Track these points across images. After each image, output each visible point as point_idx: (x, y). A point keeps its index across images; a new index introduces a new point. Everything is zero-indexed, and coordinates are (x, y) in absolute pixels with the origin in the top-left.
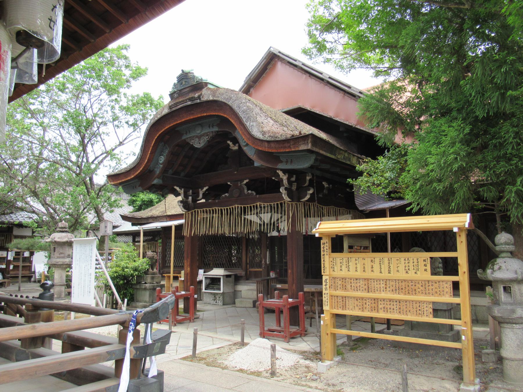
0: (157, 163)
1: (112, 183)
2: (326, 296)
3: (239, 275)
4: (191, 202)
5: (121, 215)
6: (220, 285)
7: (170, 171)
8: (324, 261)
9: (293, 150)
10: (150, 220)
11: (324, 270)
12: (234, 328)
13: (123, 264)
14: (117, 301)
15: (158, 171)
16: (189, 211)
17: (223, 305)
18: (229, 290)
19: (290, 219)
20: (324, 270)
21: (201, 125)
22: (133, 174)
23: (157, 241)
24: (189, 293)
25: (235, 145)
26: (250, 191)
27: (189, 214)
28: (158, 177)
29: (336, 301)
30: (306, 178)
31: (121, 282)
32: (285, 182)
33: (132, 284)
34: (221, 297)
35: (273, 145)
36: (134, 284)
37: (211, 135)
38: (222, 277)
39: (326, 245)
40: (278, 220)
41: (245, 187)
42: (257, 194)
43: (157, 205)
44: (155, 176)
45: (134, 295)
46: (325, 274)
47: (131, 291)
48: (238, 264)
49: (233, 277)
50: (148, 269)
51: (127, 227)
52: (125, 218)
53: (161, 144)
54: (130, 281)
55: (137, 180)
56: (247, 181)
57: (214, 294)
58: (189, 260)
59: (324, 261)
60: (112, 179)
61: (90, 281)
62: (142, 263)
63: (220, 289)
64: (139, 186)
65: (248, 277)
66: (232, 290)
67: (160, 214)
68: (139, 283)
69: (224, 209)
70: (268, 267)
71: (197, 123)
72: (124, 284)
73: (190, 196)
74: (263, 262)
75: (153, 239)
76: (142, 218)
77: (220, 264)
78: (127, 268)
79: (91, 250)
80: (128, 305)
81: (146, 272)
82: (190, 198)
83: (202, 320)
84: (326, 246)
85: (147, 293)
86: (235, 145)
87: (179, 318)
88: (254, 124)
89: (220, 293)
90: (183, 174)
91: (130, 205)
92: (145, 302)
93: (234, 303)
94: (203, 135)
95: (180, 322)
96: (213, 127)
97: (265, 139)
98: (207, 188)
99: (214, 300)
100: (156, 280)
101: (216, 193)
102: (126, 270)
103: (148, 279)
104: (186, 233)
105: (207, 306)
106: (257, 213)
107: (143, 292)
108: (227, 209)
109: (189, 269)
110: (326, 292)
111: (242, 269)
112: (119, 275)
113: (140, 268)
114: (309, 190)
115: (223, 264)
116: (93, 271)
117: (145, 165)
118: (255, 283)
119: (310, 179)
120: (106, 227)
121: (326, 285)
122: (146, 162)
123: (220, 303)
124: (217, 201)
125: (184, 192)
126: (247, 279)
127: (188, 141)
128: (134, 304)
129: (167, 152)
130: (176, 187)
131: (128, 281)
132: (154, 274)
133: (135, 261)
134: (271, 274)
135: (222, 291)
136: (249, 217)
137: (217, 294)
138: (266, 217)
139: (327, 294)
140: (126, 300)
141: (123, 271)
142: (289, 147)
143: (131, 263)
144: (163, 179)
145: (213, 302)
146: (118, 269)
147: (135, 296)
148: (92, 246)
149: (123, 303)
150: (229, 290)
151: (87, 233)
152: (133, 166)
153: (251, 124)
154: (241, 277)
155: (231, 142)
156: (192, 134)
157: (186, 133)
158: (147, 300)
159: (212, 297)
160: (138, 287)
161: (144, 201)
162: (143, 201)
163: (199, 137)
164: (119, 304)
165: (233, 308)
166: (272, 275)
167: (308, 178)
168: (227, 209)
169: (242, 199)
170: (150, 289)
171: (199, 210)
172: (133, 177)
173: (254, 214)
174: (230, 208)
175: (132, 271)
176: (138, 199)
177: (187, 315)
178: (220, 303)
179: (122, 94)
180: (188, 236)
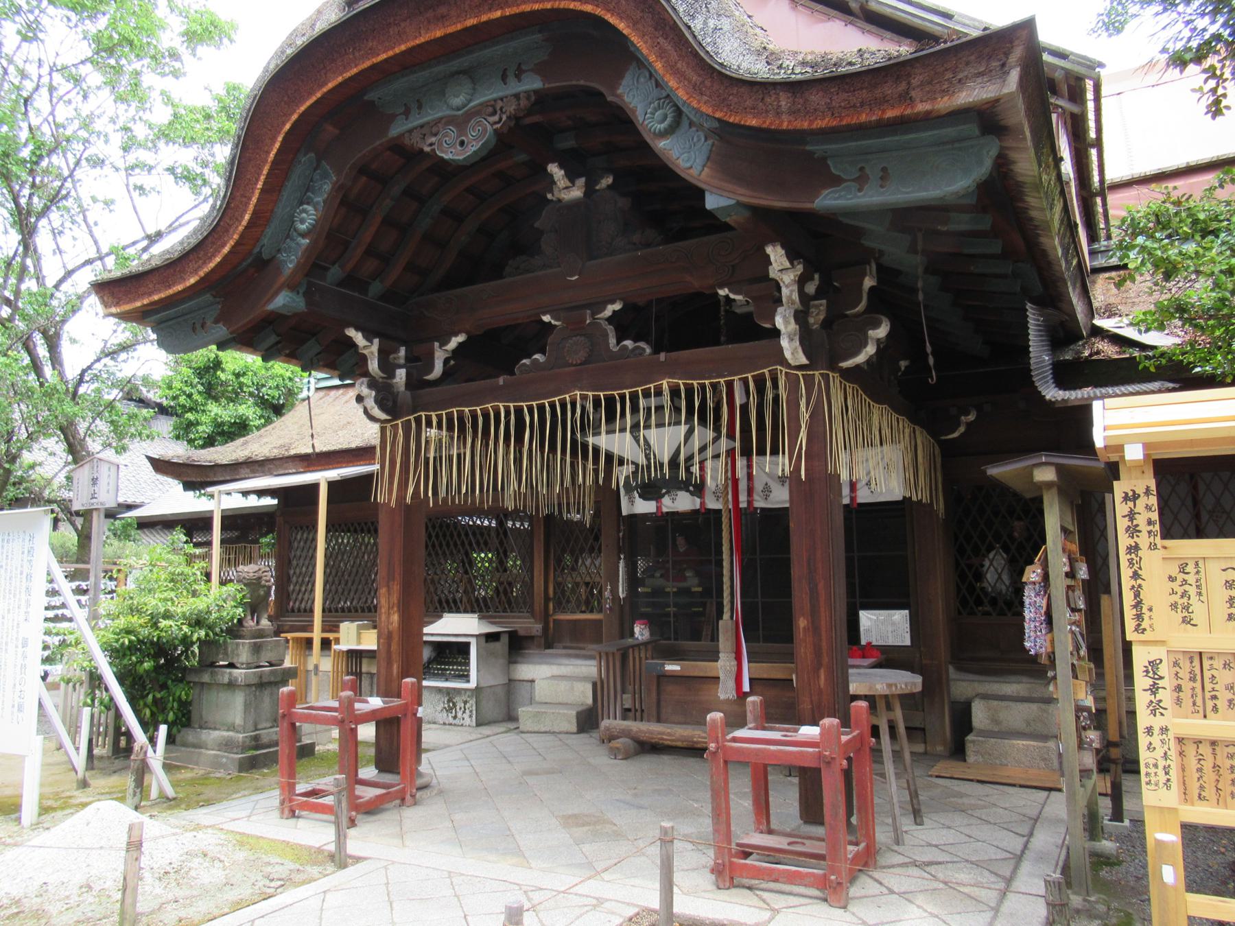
0: (289, 230)
1: (114, 310)
2: (1156, 739)
3: (522, 633)
4: (402, 388)
5: (150, 459)
6: (468, 664)
7: (335, 272)
8: (1136, 576)
9: (922, 107)
10: (244, 471)
11: (1139, 617)
12: (579, 832)
13: (153, 603)
14: (129, 735)
15: (290, 263)
16: (395, 419)
17: (479, 724)
18: (495, 679)
19: (803, 435)
20: (1139, 617)
21: (471, 75)
22: (196, 271)
23: (256, 542)
24: (397, 702)
25: (572, 181)
26: (628, 343)
27: (395, 427)
28: (292, 286)
29: (1208, 765)
30: (861, 284)
31: (147, 665)
32: (789, 292)
33: (185, 670)
34: (472, 702)
35: (816, 98)
36: (193, 670)
37: (511, 108)
38: (473, 641)
39: (1141, 503)
40: (703, 449)
41: (610, 329)
42: (656, 351)
43: (256, 433)
44: (282, 279)
45: (190, 703)
46: (1148, 636)
47: (181, 692)
48: (523, 604)
49: (505, 639)
50: (240, 621)
51: (175, 499)
52: (161, 466)
53: (307, 158)
54: (178, 658)
55: (208, 297)
56: (617, 306)
57: (449, 693)
58: (396, 588)
59: (1136, 576)
60: (113, 294)
61: (24, 667)
62: (219, 598)
63: (465, 677)
64: (216, 321)
65: (551, 640)
66: (501, 680)
67: (276, 453)
68: (208, 664)
69: (530, 409)
70: (622, 607)
71: (455, 65)
72: (157, 668)
73: (400, 367)
74: (607, 594)
75: (243, 538)
76: (217, 466)
77: (447, 602)
78: (167, 615)
79: (30, 551)
80: (171, 740)
81: (235, 630)
82: (401, 374)
83: (441, 792)
84: (1133, 507)
85: (239, 699)
86: (572, 181)
87: (368, 793)
88: (725, 24)
89: (466, 690)
90: (376, 288)
91: (178, 438)
92: (232, 728)
93: (511, 717)
94: (477, 112)
95: (371, 809)
96: (518, 77)
97: (781, 76)
98: (461, 338)
99: (449, 710)
100: (267, 656)
101: (496, 354)
102: (164, 623)
103: (243, 651)
104: (384, 495)
105: (449, 745)
106: (635, 427)
107: (224, 696)
108: (541, 408)
109: (395, 618)
110: (1157, 722)
111: (533, 616)
112: (140, 642)
113: (214, 616)
114: (876, 325)
115: (455, 601)
116: (35, 631)
117: (242, 236)
118: (591, 657)
119: (872, 289)
120: (94, 481)
121: (1154, 689)
122: (244, 223)
123: (467, 721)
124: (501, 381)
125: (380, 351)
126: (549, 645)
127: (415, 141)
128: (189, 735)
129: (327, 187)
130: (351, 333)
131: (172, 662)
132: (260, 634)
133: (194, 594)
134: (637, 629)
135: (472, 684)
136: (604, 441)
137: (458, 691)
138: (665, 440)
139: (1164, 730)
140: (163, 729)
141: (155, 625)
142: (905, 98)
143: (182, 600)
144: (308, 295)
145: (444, 717)
146: (135, 620)
147: (194, 709)
148: (32, 538)
149: (153, 741)
150: (495, 679)
151: (420, 788)
152: (194, 241)
153: (711, 23)
154: (532, 638)
155: (561, 166)
156: (430, 115)
157: (407, 113)
158: (239, 720)
159: (441, 703)
160: (206, 678)
161: (222, 424)
162: (218, 425)
163: (461, 122)
164: (136, 747)
165: (512, 737)
166: (640, 632)
167: (868, 283)
168: (541, 408)
169: (596, 368)
170: (249, 686)
171: (433, 414)
172: (192, 281)
173: (623, 430)
174: (552, 406)
175: (185, 628)
176: (203, 419)
177: (388, 778)
178: (468, 720)
179: (155, 95)
180: (393, 504)
